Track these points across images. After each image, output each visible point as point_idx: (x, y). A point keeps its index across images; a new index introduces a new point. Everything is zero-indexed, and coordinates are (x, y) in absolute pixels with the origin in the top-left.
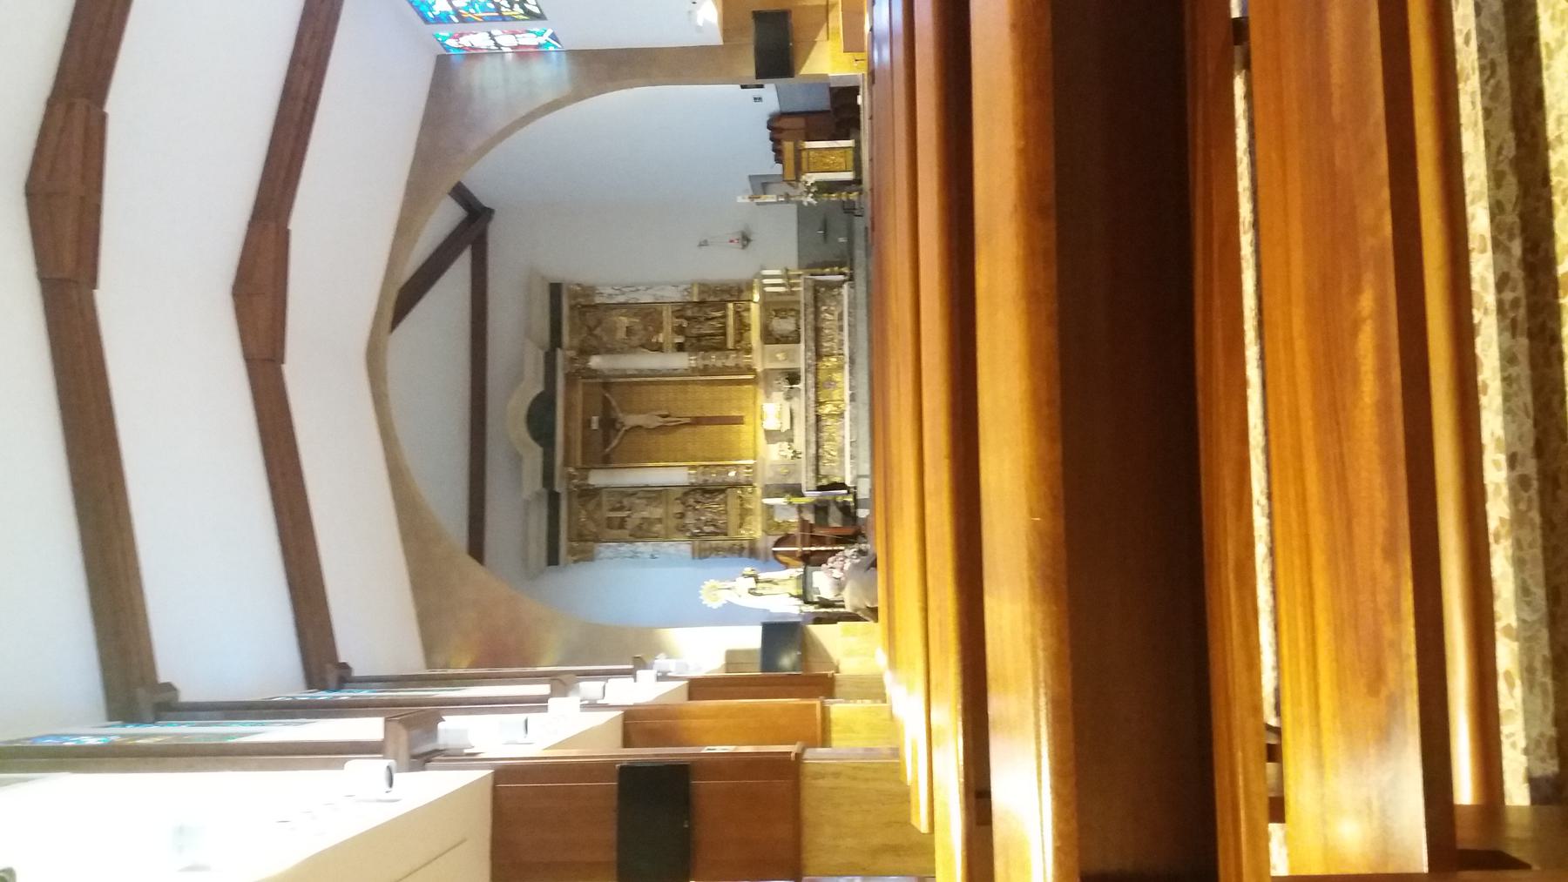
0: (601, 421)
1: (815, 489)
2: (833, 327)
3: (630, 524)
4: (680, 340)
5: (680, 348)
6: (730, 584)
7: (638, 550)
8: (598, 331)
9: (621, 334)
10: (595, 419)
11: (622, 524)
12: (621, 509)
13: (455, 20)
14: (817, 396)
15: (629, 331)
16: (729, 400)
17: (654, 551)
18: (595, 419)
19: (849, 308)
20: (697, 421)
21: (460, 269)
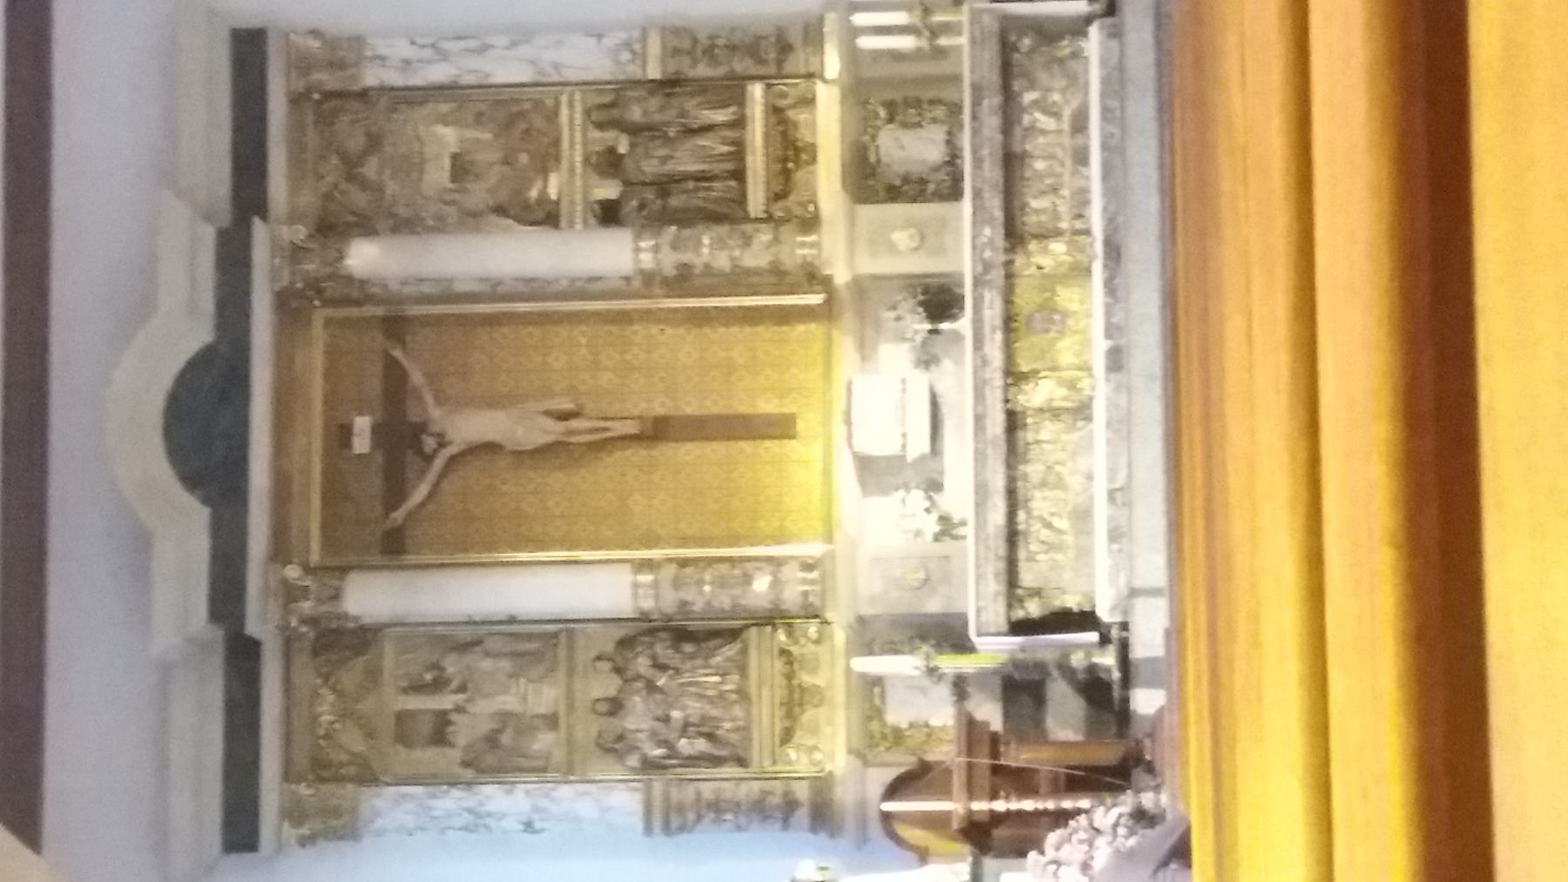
3: (465, 732)
4: (609, 190)
8: (370, 169)
17: (536, 809)
20: (659, 430)
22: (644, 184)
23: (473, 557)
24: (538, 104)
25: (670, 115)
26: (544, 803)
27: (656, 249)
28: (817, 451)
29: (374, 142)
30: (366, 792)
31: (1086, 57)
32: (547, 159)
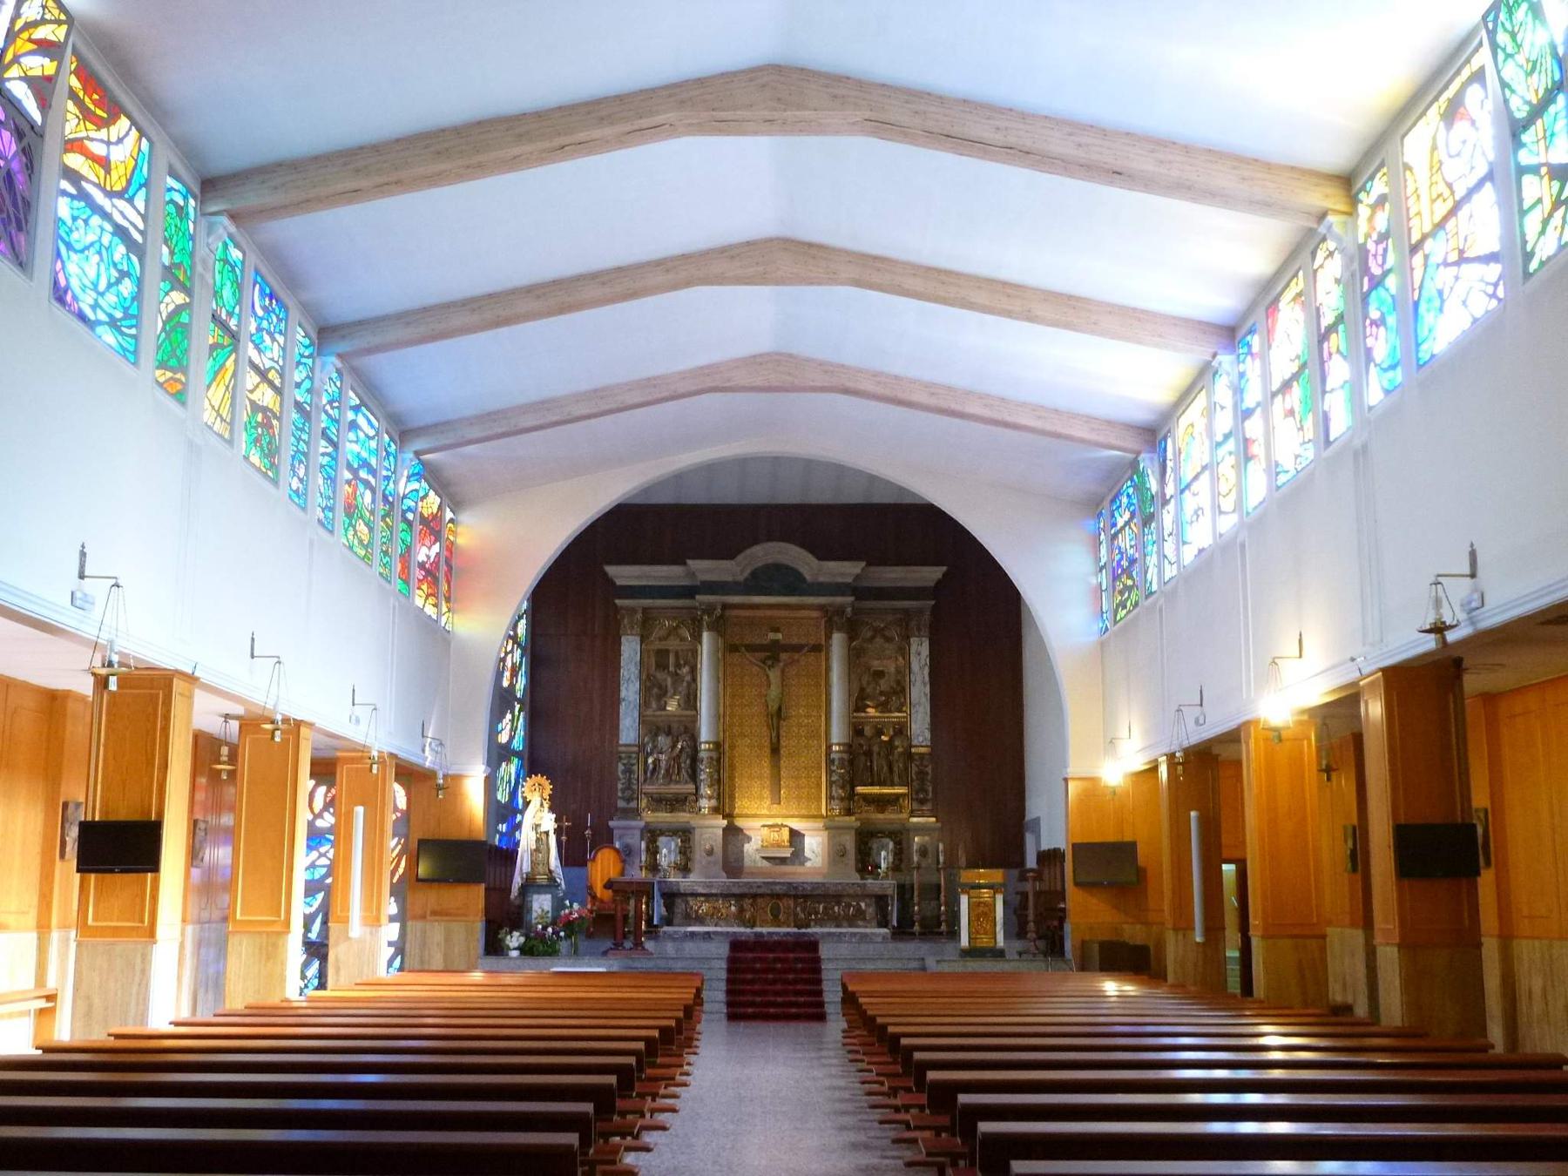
0: (776, 642)
1: (1292, 418)
2: (1380, 251)
3: (660, 675)
4: (868, 731)
5: (857, 730)
6: (546, 806)
7: (631, 685)
8: (879, 640)
9: (876, 665)
10: (779, 636)
11: (662, 666)
12: (678, 666)
13: (1113, 532)
14: (762, 895)
15: (880, 674)
16: (798, 787)
17: (630, 702)
18: (779, 636)
19: (861, 933)
20: (775, 750)
21: (143, 212)
22: (1520, 714)
23: (582, 136)
24: (903, 705)
25: (896, 756)
26: (632, 706)
27: (709, 750)
28: (765, 812)
29: (889, 640)
30: (638, 639)
31: (826, 829)
32: (883, 707)
